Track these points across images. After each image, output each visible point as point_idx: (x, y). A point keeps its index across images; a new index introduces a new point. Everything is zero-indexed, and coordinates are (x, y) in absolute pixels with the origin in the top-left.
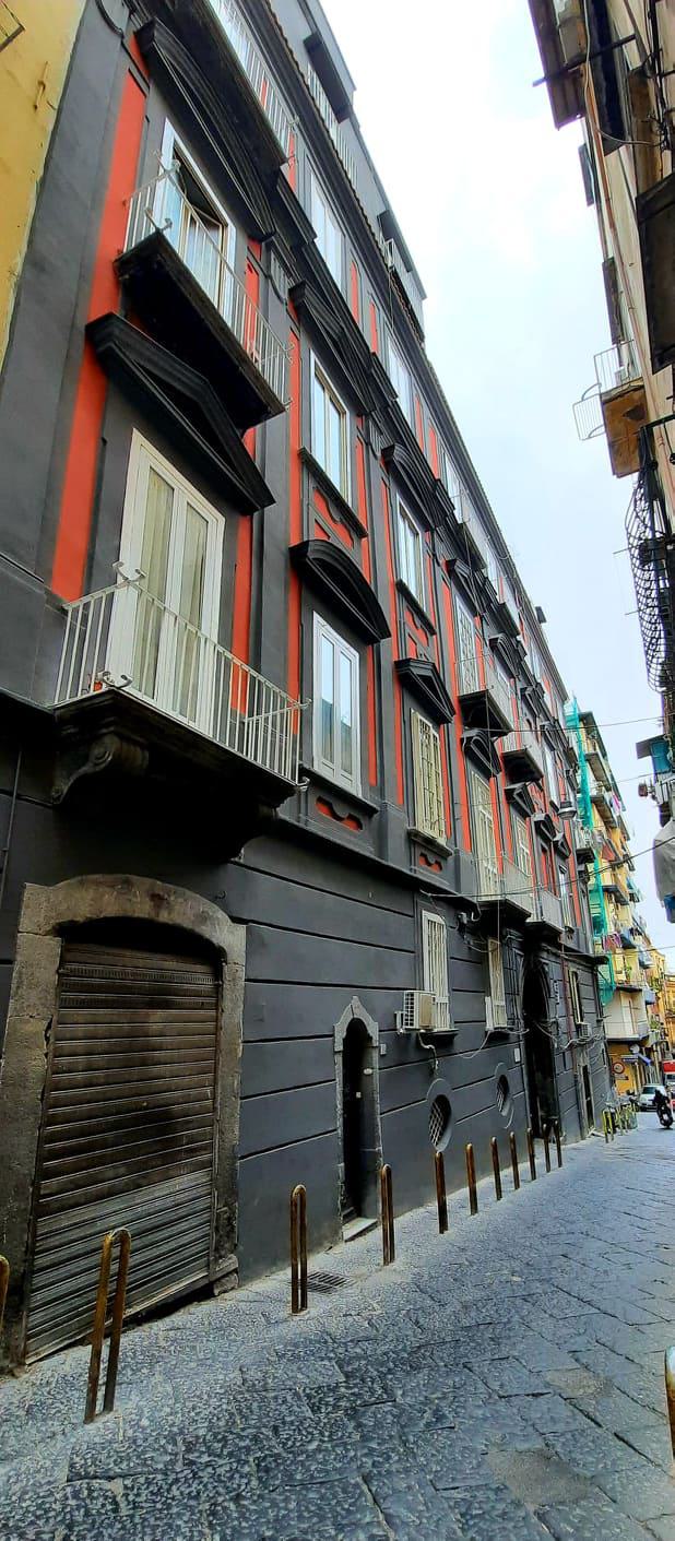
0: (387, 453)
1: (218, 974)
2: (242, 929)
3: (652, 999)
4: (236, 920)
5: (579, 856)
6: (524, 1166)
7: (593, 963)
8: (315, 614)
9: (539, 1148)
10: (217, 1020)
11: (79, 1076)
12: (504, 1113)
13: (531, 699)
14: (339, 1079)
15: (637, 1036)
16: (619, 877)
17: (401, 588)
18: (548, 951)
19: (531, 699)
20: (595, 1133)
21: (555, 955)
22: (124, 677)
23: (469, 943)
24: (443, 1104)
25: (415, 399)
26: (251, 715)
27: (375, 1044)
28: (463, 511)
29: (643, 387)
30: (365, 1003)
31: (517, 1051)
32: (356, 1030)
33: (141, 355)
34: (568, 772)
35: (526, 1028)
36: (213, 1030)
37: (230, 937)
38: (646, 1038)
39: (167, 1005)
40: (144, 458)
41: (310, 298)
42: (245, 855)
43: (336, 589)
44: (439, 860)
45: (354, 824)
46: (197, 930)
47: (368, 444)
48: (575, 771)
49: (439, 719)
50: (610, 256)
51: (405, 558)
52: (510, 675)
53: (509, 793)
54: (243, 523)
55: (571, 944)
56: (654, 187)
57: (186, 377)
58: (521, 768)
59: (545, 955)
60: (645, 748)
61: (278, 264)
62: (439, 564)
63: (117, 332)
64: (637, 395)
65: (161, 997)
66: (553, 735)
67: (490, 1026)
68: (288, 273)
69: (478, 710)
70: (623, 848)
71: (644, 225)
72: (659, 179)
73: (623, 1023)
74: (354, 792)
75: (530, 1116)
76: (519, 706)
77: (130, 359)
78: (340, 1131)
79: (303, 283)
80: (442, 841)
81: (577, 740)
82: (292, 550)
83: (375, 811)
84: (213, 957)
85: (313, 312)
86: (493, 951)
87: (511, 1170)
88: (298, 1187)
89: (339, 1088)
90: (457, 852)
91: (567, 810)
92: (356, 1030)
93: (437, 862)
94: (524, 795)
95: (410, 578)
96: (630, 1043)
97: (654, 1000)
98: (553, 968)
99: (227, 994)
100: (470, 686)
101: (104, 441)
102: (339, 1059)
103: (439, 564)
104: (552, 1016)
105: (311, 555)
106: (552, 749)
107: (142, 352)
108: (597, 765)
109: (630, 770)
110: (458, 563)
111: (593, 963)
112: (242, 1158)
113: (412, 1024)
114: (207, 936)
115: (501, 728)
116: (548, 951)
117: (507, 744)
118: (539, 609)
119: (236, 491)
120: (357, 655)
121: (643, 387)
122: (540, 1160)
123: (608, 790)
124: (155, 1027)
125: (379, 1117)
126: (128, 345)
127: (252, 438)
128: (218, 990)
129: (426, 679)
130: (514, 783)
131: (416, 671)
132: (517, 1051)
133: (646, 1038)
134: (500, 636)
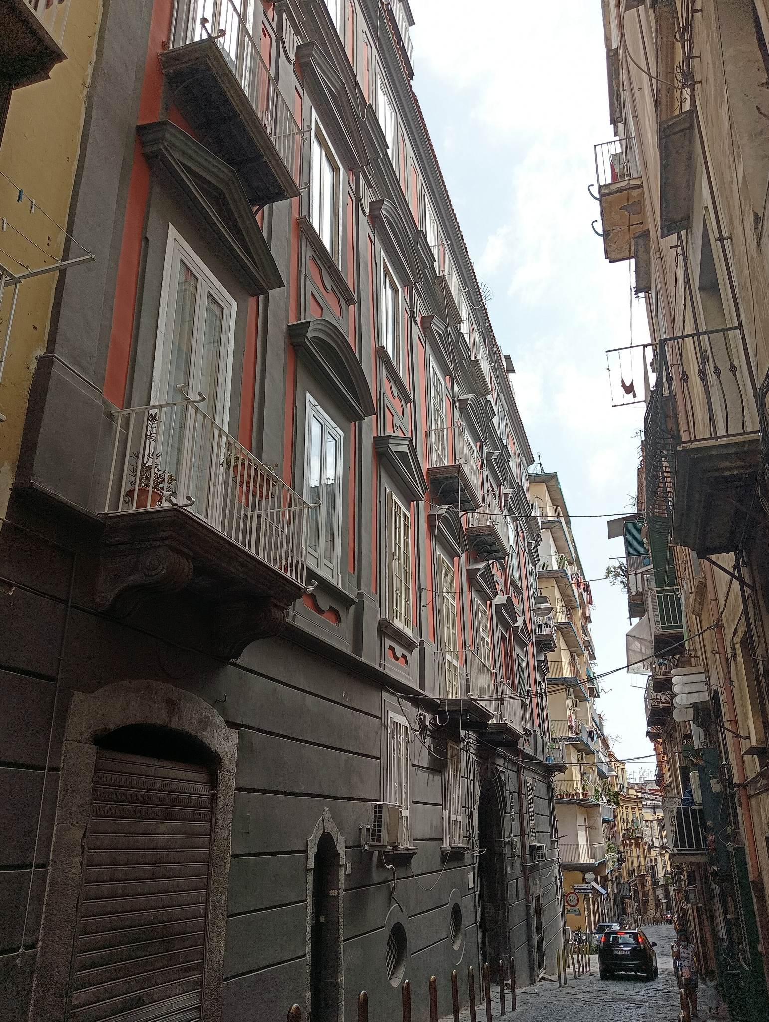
0: (375, 206)
1: (213, 783)
2: (235, 734)
3: (610, 817)
4: (232, 725)
5: (538, 643)
6: (481, 1009)
7: (549, 770)
8: (308, 395)
9: (495, 990)
10: (211, 833)
11: (105, 887)
12: (456, 947)
13: (497, 465)
14: (309, 900)
15: (593, 861)
16: (579, 666)
17: (381, 353)
18: (505, 757)
19: (497, 465)
20: (545, 976)
21: (511, 761)
22: (188, 498)
23: (430, 746)
24: (398, 936)
25: (400, 137)
26: (253, 510)
27: (342, 862)
28: (444, 265)
29: (641, 186)
30: (335, 816)
31: (471, 875)
32: (326, 842)
33: (183, 153)
34: (529, 545)
35: (481, 846)
36: (207, 844)
37: (224, 742)
38: (603, 864)
39: (170, 816)
40: (177, 249)
41: (315, 57)
42: (249, 657)
43: (334, 372)
44: (406, 653)
45: (333, 618)
46: (199, 736)
47: (358, 199)
48: (537, 545)
49: (410, 496)
50: (614, 48)
51: (388, 319)
52: (477, 439)
53: (471, 574)
54: (252, 301)
55: (529, 750)
56: (672, 118)
57: (216, 169)
58: (484, 546)
59: (501, 761)
60: (617, 527)
61: (289, 24)
62: (416, 323)
63: (167, 136)
64: (635, 193)
65: (170, 808)
66: (517, 506)
67: (446, 845)
68: (297, 32)
69: (448, 488)
70: (584, 632)
71: (664, 141)
72: (677, 112)
73: (581, 846)
74: (333, 582)
75: (481, 952)
76: (485, 472)
77: (175, 157)
78: (308, 957)
79: (312, 44)
80: (409, 632)
81: (539, 503)
82: (290, 328)
83: (352, 602)
84: (206, 760)
85: (318, 70)
86: (451, 758)
87: (484, 1006)
88: (295, 1005)
89: (309, 910)
90: (422, 642)
91: (543, 605)
92: (326, 842)
93: (331, 609)
94: (488, 575)
95: (387, 342)
96: (585, 869)
97: (611, 819)
98: (509, 778)
99: (221, 804)
100: (442, 460)
101: (147, 240)
102: (310, 878)
103: (416, 323)
104: (507, 834)
105: (310, 335)
106: (515, 519)
107: (185, 150)
108: (559, 534)
109: (600, 553)
110: (435, 320)
111: (549, 770)
112: (226, 980)
113: (379, 841)
114: (207, 742)
115: (470, 504)
116: (505, 757)
117: (472, 521)
118: (508, 358)
119: (247, 269)
120: (342, 433)
121: (641, 186)
122: (495, 1005)
123: (570, 563)
124: (162, 840)
125: (342, 943)
126: (173, 145)
127: (262, 216)
128: (213, 798)
129: (403, 455)
130: (476, 561)
131: (394, 448)
132: (471, 875)
133: (603, 864)
134: (470, 396)
